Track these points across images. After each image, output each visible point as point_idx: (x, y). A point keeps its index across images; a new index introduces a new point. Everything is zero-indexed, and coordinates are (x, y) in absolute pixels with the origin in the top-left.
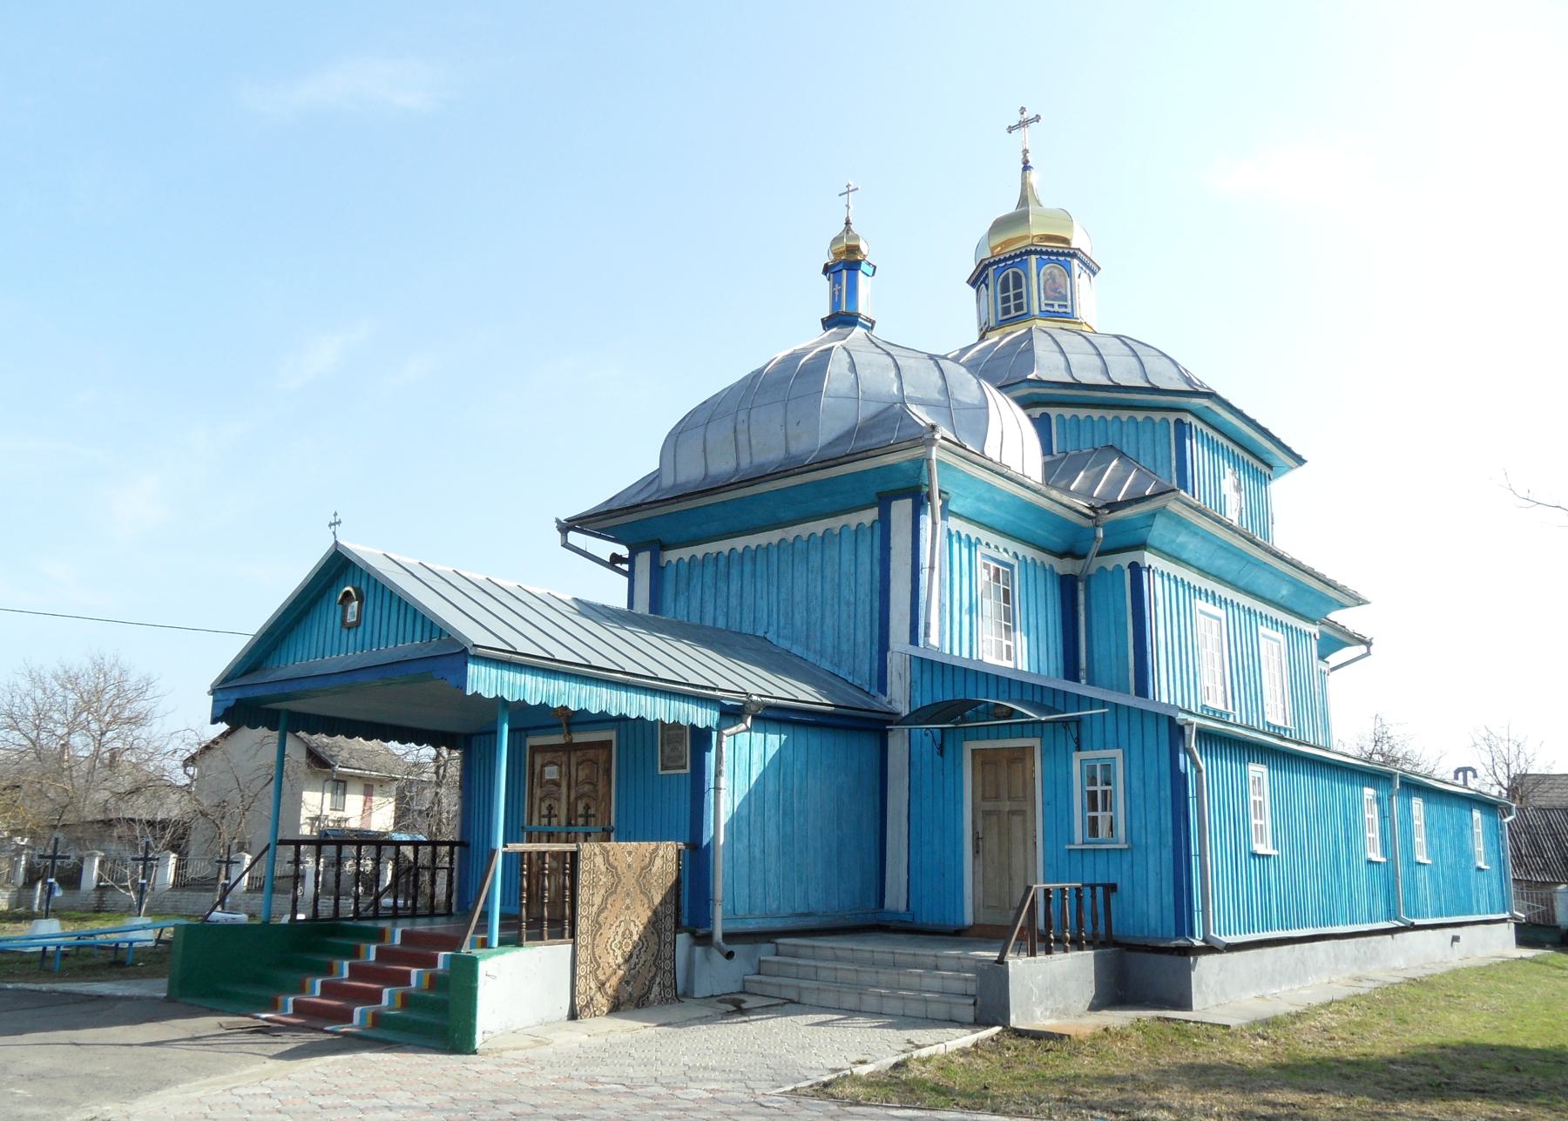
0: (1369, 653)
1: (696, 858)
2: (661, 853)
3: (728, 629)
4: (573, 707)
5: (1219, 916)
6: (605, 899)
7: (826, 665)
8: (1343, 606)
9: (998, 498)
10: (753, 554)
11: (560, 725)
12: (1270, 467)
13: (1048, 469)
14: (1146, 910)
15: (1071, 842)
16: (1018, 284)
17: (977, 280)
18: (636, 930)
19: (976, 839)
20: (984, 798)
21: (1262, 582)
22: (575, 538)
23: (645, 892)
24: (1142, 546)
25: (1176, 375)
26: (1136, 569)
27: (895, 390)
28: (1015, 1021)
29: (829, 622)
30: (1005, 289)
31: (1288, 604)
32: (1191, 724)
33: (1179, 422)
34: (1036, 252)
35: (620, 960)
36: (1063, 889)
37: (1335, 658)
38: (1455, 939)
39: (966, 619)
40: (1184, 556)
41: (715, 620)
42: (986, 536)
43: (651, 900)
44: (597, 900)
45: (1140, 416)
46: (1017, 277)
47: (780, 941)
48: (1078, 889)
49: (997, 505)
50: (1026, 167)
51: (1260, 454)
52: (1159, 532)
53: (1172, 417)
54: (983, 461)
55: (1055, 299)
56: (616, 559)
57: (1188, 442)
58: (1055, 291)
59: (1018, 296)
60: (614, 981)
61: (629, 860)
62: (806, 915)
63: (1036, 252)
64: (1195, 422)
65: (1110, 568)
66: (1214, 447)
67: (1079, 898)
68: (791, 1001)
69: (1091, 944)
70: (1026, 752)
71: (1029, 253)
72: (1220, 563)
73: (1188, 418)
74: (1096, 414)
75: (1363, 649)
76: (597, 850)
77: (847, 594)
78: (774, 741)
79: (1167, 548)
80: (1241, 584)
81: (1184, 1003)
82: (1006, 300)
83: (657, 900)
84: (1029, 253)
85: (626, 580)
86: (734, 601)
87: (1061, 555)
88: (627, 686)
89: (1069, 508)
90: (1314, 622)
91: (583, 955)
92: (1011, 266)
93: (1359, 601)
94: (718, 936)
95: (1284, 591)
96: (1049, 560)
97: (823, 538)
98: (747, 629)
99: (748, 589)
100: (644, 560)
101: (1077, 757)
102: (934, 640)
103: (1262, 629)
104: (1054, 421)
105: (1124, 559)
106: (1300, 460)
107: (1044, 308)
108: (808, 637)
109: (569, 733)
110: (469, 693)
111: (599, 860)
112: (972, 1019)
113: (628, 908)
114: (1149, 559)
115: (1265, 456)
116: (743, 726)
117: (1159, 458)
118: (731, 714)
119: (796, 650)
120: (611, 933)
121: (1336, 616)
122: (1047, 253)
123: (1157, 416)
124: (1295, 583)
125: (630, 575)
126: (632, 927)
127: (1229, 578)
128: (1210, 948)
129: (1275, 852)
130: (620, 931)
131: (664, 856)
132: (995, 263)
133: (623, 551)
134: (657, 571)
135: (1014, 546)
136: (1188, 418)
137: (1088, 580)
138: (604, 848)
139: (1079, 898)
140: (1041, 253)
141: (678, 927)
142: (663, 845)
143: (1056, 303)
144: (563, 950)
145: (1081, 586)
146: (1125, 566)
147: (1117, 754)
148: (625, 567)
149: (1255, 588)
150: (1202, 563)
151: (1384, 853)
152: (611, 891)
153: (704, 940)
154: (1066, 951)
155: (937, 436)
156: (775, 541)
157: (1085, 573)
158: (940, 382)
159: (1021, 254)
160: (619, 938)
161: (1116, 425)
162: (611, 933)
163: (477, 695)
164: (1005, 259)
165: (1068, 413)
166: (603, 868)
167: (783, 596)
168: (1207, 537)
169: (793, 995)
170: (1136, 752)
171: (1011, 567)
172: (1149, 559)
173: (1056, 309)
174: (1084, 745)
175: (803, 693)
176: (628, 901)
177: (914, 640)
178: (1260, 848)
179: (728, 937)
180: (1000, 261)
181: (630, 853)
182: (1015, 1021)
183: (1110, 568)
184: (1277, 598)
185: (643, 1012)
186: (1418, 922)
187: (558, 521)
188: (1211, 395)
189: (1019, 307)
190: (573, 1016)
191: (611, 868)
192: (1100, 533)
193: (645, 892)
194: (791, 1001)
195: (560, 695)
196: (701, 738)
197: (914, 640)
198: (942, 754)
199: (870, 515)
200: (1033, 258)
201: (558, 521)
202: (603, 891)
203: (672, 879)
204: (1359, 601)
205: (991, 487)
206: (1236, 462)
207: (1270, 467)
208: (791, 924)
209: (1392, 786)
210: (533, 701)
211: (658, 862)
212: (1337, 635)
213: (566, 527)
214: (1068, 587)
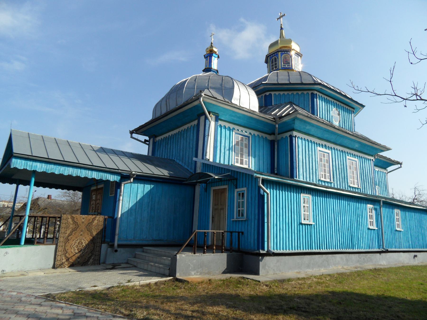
0: (401, 167)
1: (112, 221)
2: (97, 219)
3: (167, 159)
4: (56, 173)
5: (272, 244)
6: (71, 232)
7: (186, 167)
8: (384, 151)
9: (238, 115)
10: (173, 136)
11: (94, 184)
12: (354, 108)
13: (260, 107)
14: (250, 241)
15: (233, 218)
16: (276, 61)
17: (266, 62)
18: (85, 243)
19: (213, 217)
20: (215, 205)
21: (346, 142)
22: (134, 135)
23: (89, 230)
24: (293, 130)
25: (311, 79)
26: (291, 137)
27: (207, 85)
28: (178, 276)
29: (187, 154)
30: (272, 62)
31: (359, 150)
32: (260, 178)
33: (312, 93)
34: (280, 51)
35: (77, 251)
36: (214, 232)
37: (389, 169)
38: (415, 256)
39: (227, 152)
40: (311, 133)
41: (165, 156)
42: (236, 127)
43: (91, 233)
44: (68, 232)
45: (300, 93)
46: (275, 59)
47: (144, 248)
48: (222, 233)
49: (239, 118)
50: (282, 29)
51: (349, 106)
52: (297, 125)
53: (310, 92)
54: (231, 105)
55: (286, 64)
56: (146, 141)
57: (315, 100)
58: (286, 61)
59: (276, 64)
60: (74, 258)
61: (83, 220)
62: (158, 240)
63: (280, 51)
64: (318, 93)
65: (284, 137)
66: (327, 102)
67: (223, 236)
68: (135, 266)
69: (226, 250)
70: (225, 189)
71: (278, 51)
72: (326, 136)
73: (315, 92)
74: (286, 93)
75: (399, 166)
76: (69, 217)
77: (191, 146)
78: (148, 187)
79: (303, 130)
80: (338, 143)
81: (257, 273)
82: (273, 66)
83: (95, 233)
84: (278, 51)
85: (148, 146)
86: (169, 150)
87: (270, 134)
88: (81, 168)
89: (265, 118)
90: (372, 156)
91: (60, 249)
92: (273, 57)
93: (388, 149)
94: (116, 244)
95: (357, 146)
96: (264, 135)
97: (187, 130)
98: (171, 158)
99: (172, 146)
100: (152, 140)
101: (236, 190)
102: (210, 156)
103: (348, 157)
104: (273, 96)
105: (288, 134)
106: (363, 106)
107: (283, 67)
108: (183, 159)
109: (97, 186)
110: (12, 167)
111: (70, 220)
112: (168, 274)
113: (81, 235)
114: (295, 133)
115: (350, 105)
116: (129, 181)
117: (306, 104)
118: (125, 177)
119: (180, 163)
120: (73, 242)
121: (384, 154)
122: (284, 51)
123: (305, 92)
124: (360, 143)
125: (149, 145)
126: (83, 241)
127: (332, 141)
128: (269, 254)
129: (402, 230)
130: (77, 242)
131: (98, 221)
132: (270, 56)
133: (147, 138)
134: (154, 143)
135: (249, 131)
136: (315, 92)
137: (278, 141)
138: (73, 217)
139: (223, 236)
140: (282, 51)
141: (103, 242)
142: (98, 216)
143: (286, 65)
144: (53, 247)
145: (276, 143)
146: (288, 136)
147: (245, 189)
148: (148, 143)
149: (344, 144)
150: (319, 135)
151: (377, 226)
152: (74, 230)
153: (112, 246)
154: (213, 253)
155: (203, 94)
156: (177, 132)
157: (275, 140)
158: (221, 82)
159: (276, 52)
160: (77, 244)
161: (292, 96)
162: (73, 242)
163: (15, 168)
164: (272, 54)
165: (277, 93)
166: (71, 223)
167: (178, 148)
168: (317, 127)
169: (136, 265)
170: (250, 189)
171: (249, 137)
172: (295, 133)
173: (286, 67)
174: (238, 187)
175: (164, 173)
176: (82, 233)
177: (203, 158)
178: (398, 229)
179: (119, 246)
180: (271, 55)
181: (83, 218)
182: (178, 276)
183: (284, 137)
184: (355, 148)
185: (74, 267)
186: (389, 250)
187: (130, 131)
188: (320, 84)
189: (276, 67)
190: (54, 267)
191: (75, 222)
192: (277, 126)
193: (89, 230)
194: (135, 266)
195: (52, 169)
196: (118, 185)
197: (203, 158)
198: (206, 191)
199: (196, 122)
200: (280, 53)
201: (130, 131)
202: (71, 230)
203: (101, 228)
204: (388, 149)
205: (234, 112)
206: (337, 107)
207: (354, 108)
208: (150, 243)
209: (380, 204)
210: (89, 177)
211: (96, 222)
212: (390, 162)
213: (132, 133)
214: (272, 143)
